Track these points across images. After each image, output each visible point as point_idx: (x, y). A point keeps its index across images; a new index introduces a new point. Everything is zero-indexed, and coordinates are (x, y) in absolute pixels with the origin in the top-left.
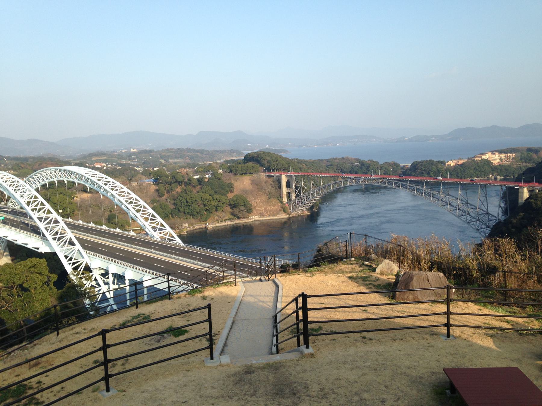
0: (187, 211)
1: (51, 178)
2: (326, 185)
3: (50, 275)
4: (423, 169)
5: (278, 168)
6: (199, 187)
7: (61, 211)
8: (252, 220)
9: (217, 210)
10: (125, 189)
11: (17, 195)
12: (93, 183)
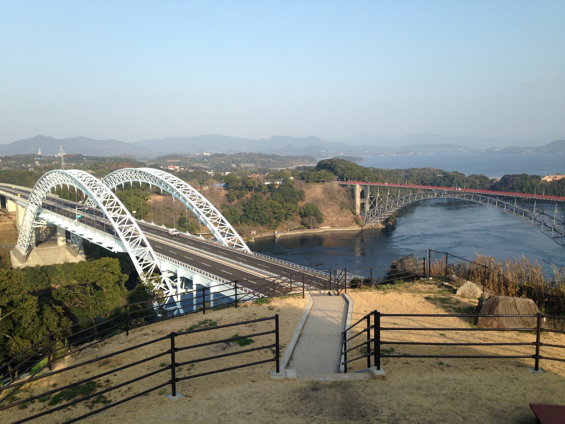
0: (256, 218)
1: (127, 178)
2: (404, 197)
3: (121, 275)
4: (515, 183)
5: (352, 176)
7: (134, 212)
8: (322, 231)
9: (286, 219)
10: (197, 193)
11: (94, 194)
12: (166, 185)
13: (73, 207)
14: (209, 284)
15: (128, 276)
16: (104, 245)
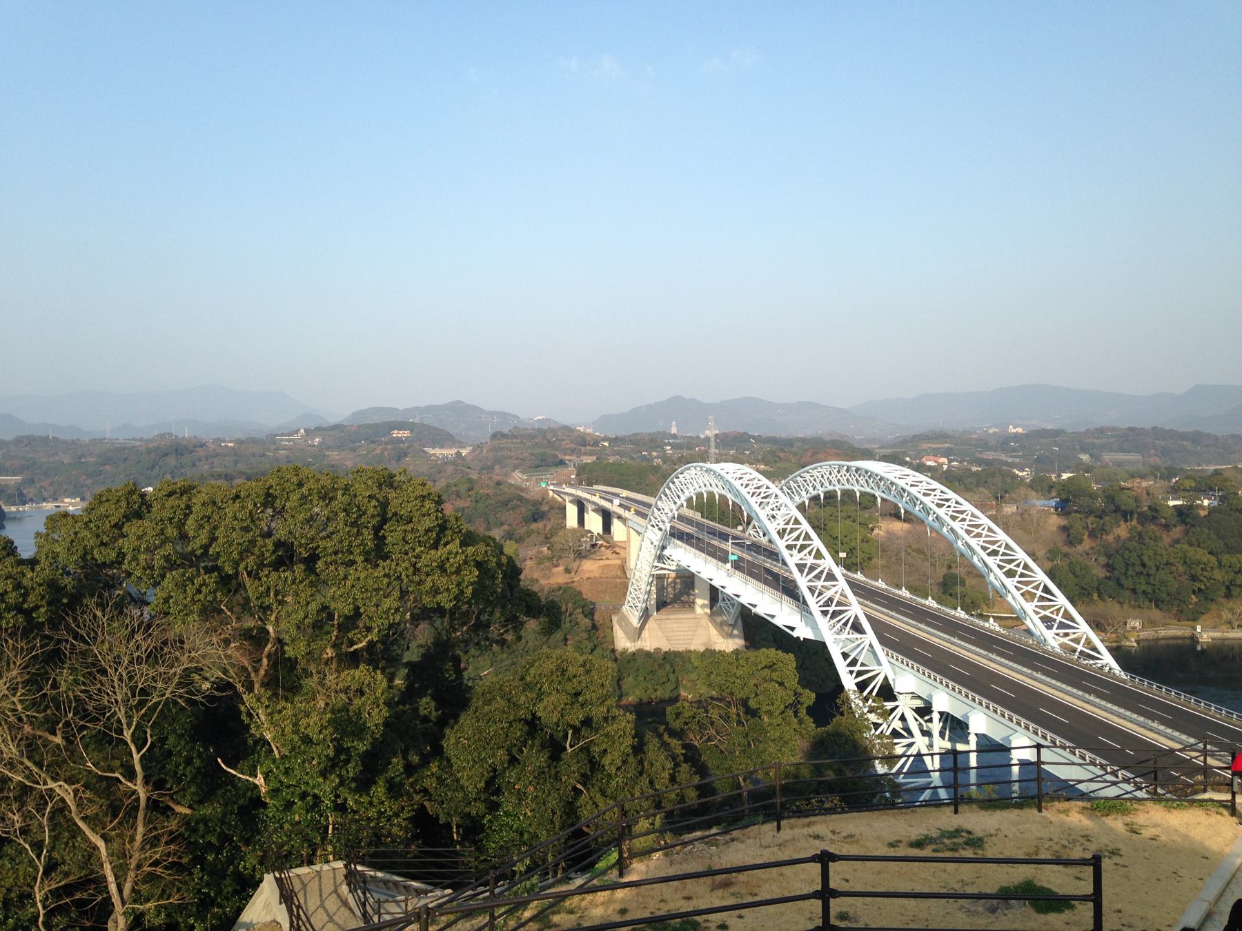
1: (830, 483)
3: (800, 690)
6: (1179, 528)
7: (843, 555)
9: (1228, 596)
10: (984, 520)
11: (763, 514)
12: (914, 500)
13: (724, 537)
14: (1007, 738)
15: (813, 695)
16: (779, 622)
